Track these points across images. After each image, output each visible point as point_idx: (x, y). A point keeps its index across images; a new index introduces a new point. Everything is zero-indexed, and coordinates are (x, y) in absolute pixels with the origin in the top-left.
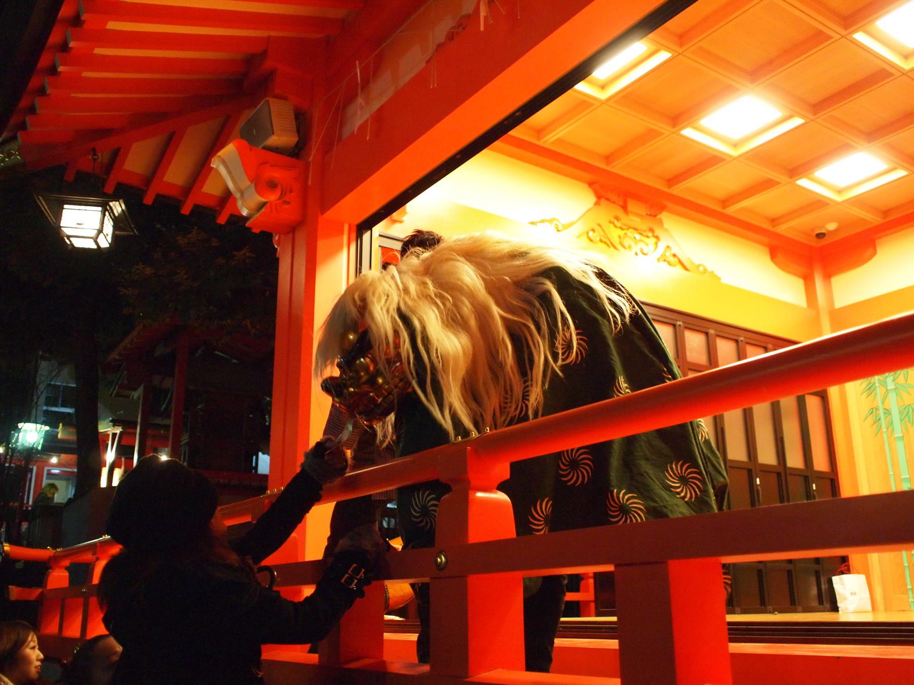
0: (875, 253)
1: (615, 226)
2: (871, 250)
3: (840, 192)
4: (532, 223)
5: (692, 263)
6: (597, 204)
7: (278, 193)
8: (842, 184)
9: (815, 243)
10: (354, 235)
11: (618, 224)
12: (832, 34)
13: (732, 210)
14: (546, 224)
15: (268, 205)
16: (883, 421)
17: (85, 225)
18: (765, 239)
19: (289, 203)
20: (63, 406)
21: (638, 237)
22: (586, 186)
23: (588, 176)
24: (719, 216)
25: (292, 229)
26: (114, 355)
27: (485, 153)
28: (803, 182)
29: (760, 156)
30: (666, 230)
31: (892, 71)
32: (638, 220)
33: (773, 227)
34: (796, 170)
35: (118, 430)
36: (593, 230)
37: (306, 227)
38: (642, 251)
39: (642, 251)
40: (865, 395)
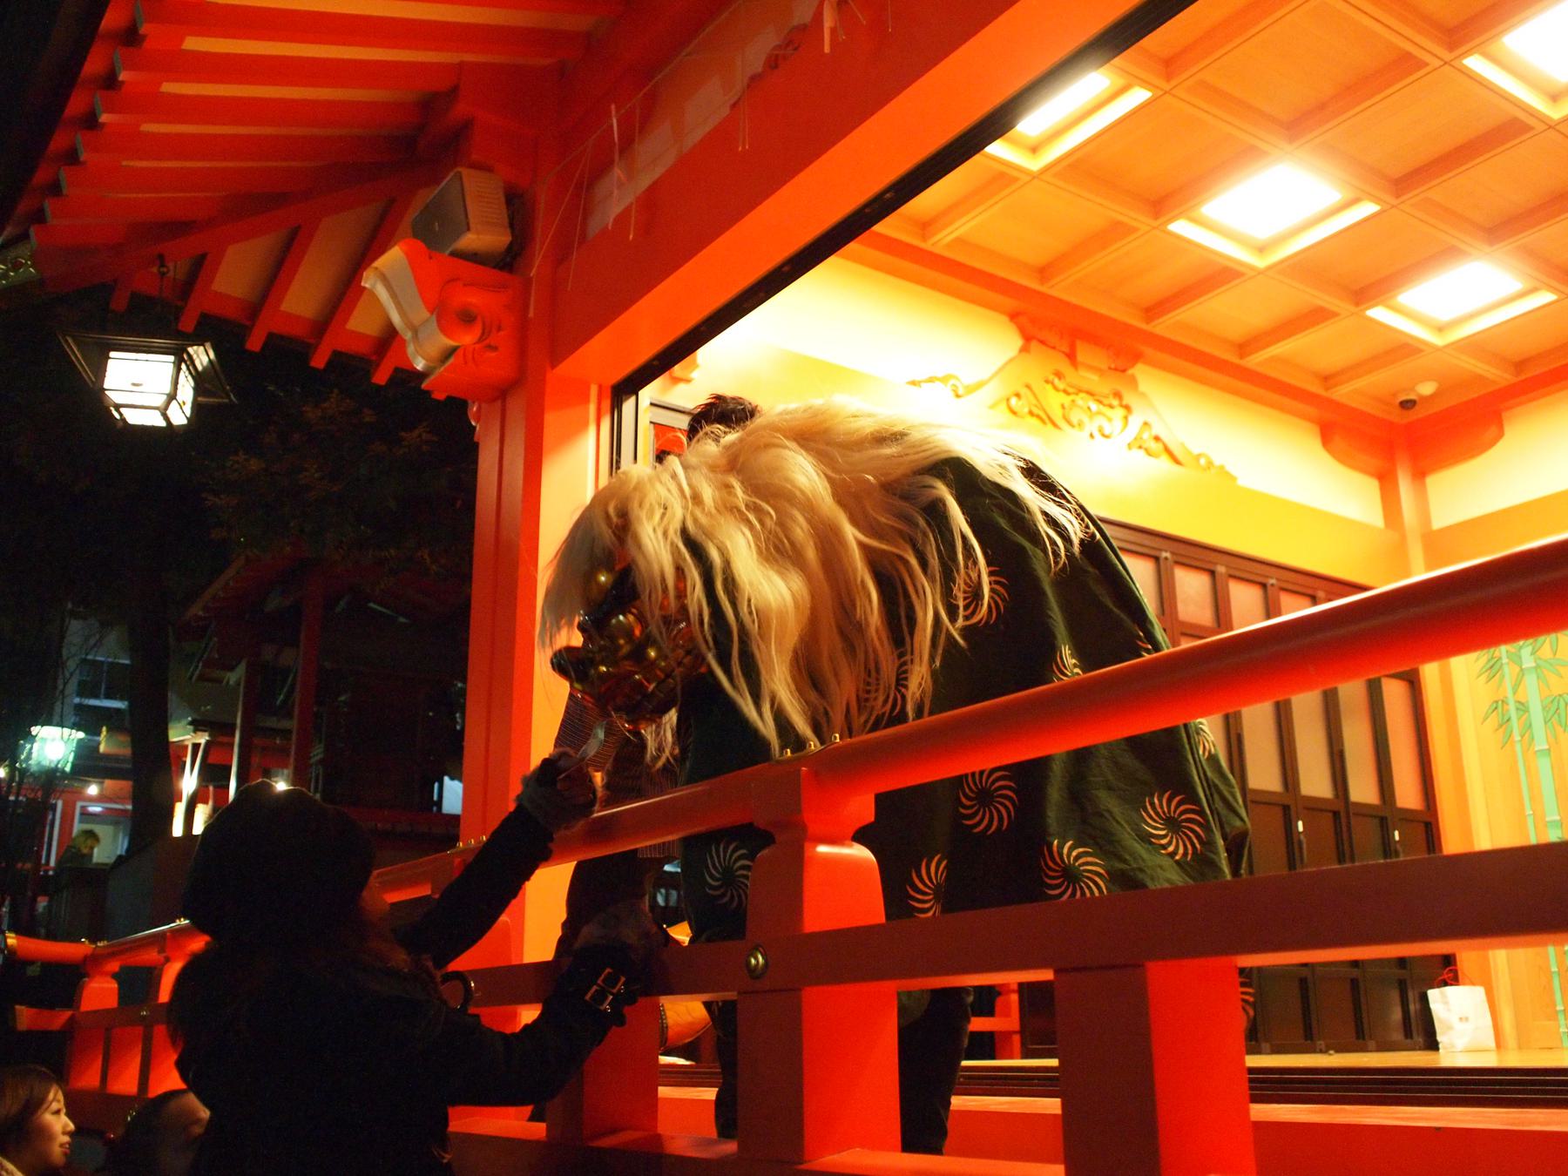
0: (1500, 435)
1: (1056, 388)
2: (1494, 429)
3: (1441, 329)
4: (913, 383)
5: (1188, 452)
6: (1024, 349)
7: (477, 331)
8: (1444, 316)
9: (1399, 417)
10: (607, 404)
11: (1061, 385)
12: (1427, 58)
13: (1255, 361)
14: (937, 384)
15: (460, 352)
16: (1515, 723)
17: (146, 387)
18: (1312, 411)
19: (496, 348)
20: (108, 697)
21: (1094, 406)
22: (1005, 319)
23: (1009, 303)
24: (1233, 370)
25: (501, 394)
26: (196, 610)
27: (832, 262)
28: (1378, 313)
29: (1303, 268)
30: (1143, 395)
31: (1531, 121)
32: (1095, 377)
33: (1327, 389)
34: (1365, 292)
35: (203, 739)
36: (1018, 395)
37: (526, 389)
38: (1101, 430)
39: (1101, 430)
40: (1483, 678)
